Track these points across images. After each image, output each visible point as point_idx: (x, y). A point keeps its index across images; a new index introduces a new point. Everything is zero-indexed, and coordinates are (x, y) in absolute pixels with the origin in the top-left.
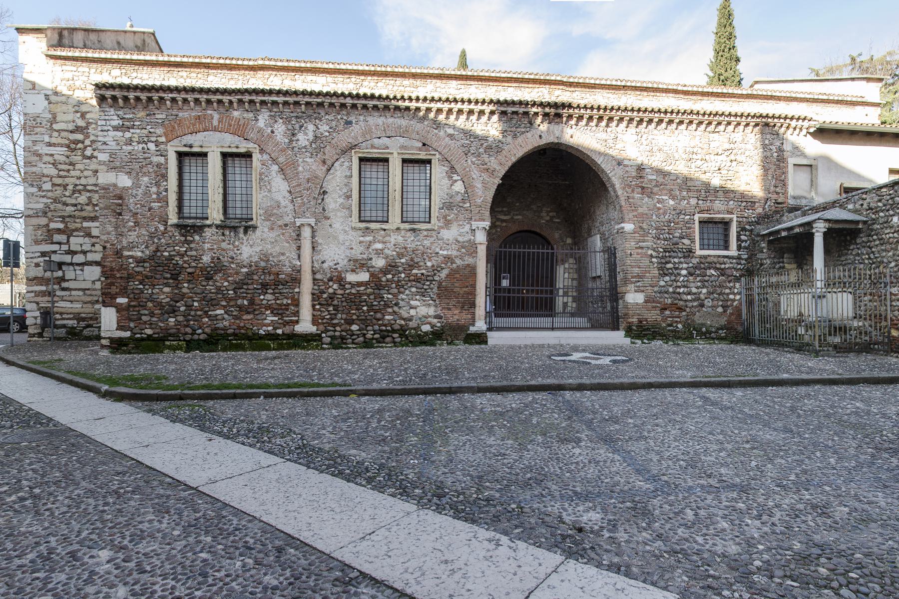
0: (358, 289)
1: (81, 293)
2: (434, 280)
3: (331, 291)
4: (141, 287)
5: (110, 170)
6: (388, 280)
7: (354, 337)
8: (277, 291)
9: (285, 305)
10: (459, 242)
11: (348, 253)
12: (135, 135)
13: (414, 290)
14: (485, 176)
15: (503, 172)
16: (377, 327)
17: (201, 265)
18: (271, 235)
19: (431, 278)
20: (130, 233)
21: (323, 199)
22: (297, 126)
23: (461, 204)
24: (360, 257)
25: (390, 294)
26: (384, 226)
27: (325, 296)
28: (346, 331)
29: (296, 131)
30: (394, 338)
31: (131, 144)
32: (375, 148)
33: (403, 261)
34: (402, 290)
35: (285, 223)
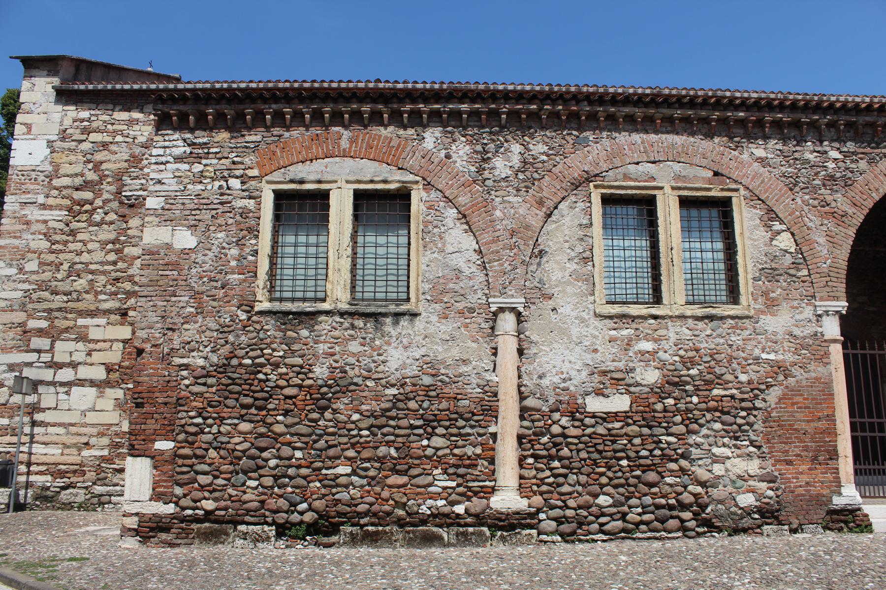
0: (610, 426)
1: (61, 430)
2: (756, 409)
3: (556, 429)
4: (199, 420)
5: (164, 223)
6: (665, 410)
7: (603, 520)
9: (469, 458)
11: (588, 358)
12: (208, 168)
13: (717, 426)
14: (830, 224)
15: (860, 218)
16: (648, 500)
17: (310, 382)
19: (749, 404)
20: (186, 326)
21: (539, 264)
22: (492, 146)
23: (792, 272)
24: (611, 366)
26: (654, 311)
27: (545, 439)
28: (587, 507)
29: (489, 155)
30: (682, 521)
31: (201, 182)
32: (631, 179)
33: (693, 372)
35: (469, 305)
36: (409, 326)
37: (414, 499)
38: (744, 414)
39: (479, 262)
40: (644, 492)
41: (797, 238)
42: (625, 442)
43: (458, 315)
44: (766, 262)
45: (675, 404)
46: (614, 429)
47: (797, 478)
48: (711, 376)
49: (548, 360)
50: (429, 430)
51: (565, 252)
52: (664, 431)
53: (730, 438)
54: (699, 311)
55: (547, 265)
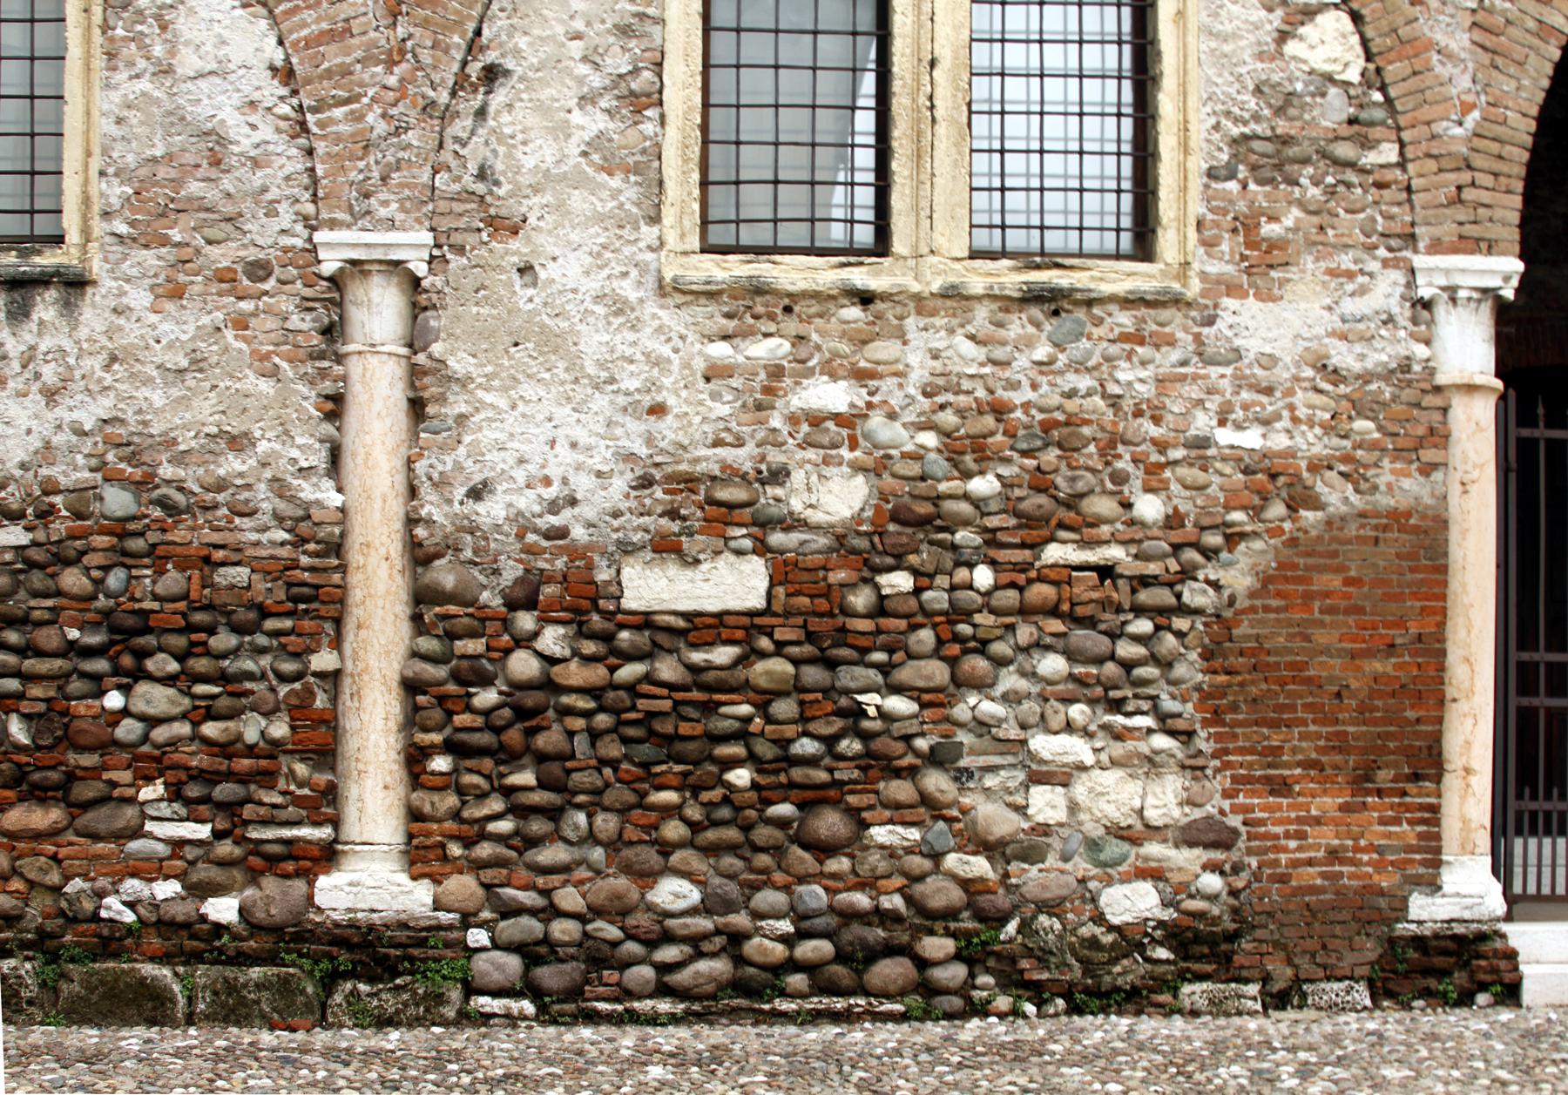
0: (697, 657)
3: (523, 665)
6: (881, 608)
7: (669, 953)
8: (201, 664)
9: (251, 750)
10: (1336, 376)
13: (1052, 664)
16: (814, 895)
18: (167, 328)
19: (1164, 596)
21: (481, 113)
23: (1344, 150)
24: (708, 460)
25: (897, 690)
26: (861, 277)
27: (487, 697)
28: (617, 911)
30: (922, 964)
33: (984, 485)
34: (979, 664)
35: (252, 254)
36: (63, 324)
37: (85, 877)
38: (1144, 626)
39: (285, 109)
40: (800, 870)
41: (1370, 32)
42: (745, 709)
43: (214, 287)
44: (1256, 118)
45: (917, 591)
46: (709, 667)
47: (1301, 836)
48: (1042, 499)
49: (502, 436)
50: (127, 661)
51: (570, 74)
52: (875, 677)
53: (1092, 702)
54: (1010, 278)
55: (506, 118)
